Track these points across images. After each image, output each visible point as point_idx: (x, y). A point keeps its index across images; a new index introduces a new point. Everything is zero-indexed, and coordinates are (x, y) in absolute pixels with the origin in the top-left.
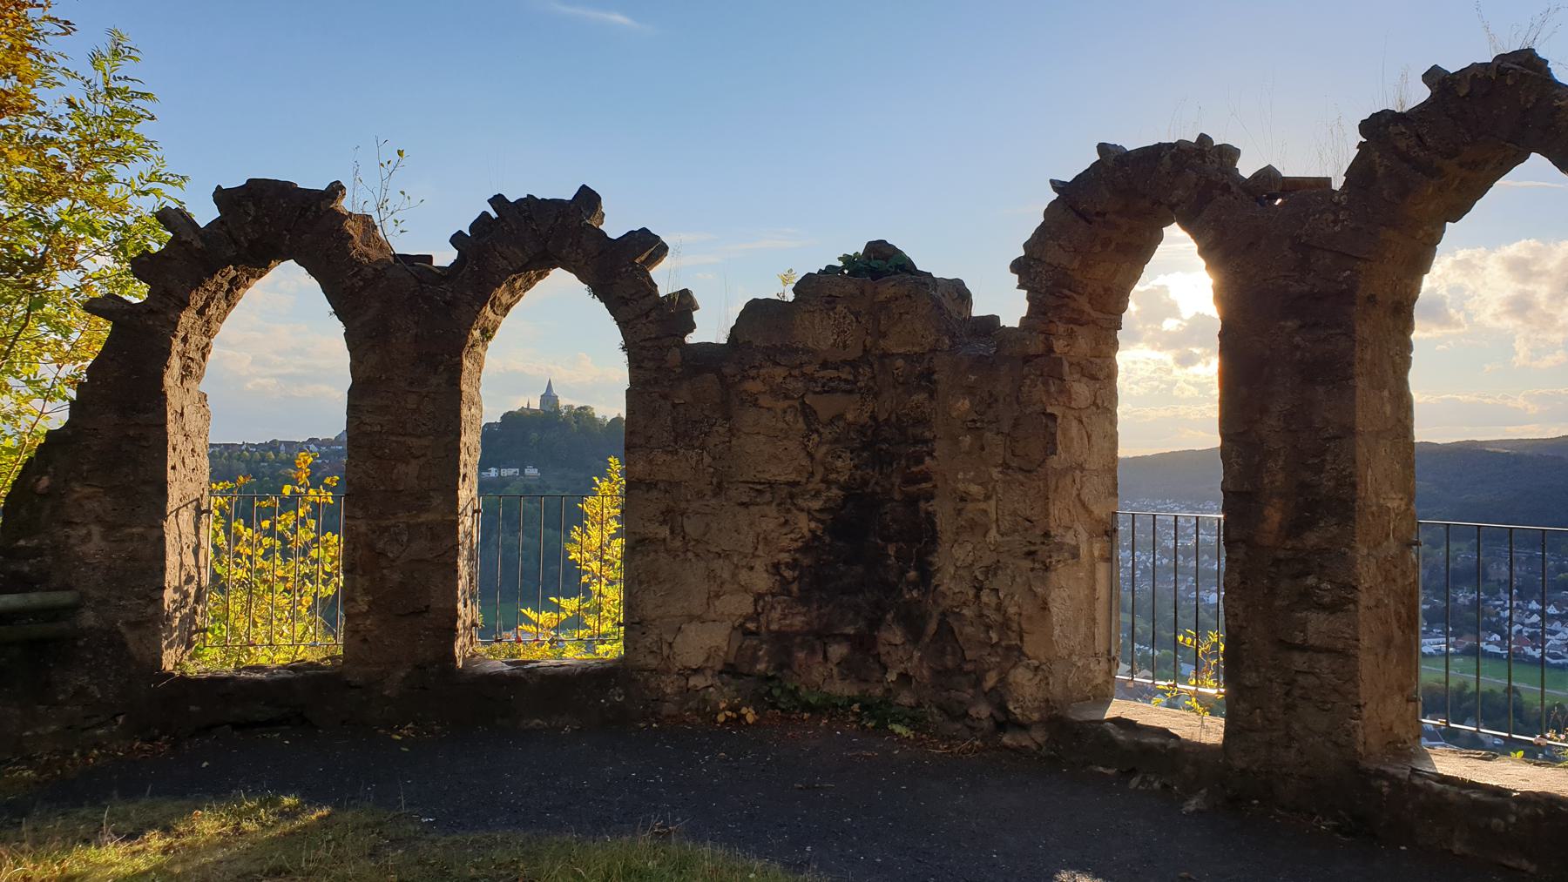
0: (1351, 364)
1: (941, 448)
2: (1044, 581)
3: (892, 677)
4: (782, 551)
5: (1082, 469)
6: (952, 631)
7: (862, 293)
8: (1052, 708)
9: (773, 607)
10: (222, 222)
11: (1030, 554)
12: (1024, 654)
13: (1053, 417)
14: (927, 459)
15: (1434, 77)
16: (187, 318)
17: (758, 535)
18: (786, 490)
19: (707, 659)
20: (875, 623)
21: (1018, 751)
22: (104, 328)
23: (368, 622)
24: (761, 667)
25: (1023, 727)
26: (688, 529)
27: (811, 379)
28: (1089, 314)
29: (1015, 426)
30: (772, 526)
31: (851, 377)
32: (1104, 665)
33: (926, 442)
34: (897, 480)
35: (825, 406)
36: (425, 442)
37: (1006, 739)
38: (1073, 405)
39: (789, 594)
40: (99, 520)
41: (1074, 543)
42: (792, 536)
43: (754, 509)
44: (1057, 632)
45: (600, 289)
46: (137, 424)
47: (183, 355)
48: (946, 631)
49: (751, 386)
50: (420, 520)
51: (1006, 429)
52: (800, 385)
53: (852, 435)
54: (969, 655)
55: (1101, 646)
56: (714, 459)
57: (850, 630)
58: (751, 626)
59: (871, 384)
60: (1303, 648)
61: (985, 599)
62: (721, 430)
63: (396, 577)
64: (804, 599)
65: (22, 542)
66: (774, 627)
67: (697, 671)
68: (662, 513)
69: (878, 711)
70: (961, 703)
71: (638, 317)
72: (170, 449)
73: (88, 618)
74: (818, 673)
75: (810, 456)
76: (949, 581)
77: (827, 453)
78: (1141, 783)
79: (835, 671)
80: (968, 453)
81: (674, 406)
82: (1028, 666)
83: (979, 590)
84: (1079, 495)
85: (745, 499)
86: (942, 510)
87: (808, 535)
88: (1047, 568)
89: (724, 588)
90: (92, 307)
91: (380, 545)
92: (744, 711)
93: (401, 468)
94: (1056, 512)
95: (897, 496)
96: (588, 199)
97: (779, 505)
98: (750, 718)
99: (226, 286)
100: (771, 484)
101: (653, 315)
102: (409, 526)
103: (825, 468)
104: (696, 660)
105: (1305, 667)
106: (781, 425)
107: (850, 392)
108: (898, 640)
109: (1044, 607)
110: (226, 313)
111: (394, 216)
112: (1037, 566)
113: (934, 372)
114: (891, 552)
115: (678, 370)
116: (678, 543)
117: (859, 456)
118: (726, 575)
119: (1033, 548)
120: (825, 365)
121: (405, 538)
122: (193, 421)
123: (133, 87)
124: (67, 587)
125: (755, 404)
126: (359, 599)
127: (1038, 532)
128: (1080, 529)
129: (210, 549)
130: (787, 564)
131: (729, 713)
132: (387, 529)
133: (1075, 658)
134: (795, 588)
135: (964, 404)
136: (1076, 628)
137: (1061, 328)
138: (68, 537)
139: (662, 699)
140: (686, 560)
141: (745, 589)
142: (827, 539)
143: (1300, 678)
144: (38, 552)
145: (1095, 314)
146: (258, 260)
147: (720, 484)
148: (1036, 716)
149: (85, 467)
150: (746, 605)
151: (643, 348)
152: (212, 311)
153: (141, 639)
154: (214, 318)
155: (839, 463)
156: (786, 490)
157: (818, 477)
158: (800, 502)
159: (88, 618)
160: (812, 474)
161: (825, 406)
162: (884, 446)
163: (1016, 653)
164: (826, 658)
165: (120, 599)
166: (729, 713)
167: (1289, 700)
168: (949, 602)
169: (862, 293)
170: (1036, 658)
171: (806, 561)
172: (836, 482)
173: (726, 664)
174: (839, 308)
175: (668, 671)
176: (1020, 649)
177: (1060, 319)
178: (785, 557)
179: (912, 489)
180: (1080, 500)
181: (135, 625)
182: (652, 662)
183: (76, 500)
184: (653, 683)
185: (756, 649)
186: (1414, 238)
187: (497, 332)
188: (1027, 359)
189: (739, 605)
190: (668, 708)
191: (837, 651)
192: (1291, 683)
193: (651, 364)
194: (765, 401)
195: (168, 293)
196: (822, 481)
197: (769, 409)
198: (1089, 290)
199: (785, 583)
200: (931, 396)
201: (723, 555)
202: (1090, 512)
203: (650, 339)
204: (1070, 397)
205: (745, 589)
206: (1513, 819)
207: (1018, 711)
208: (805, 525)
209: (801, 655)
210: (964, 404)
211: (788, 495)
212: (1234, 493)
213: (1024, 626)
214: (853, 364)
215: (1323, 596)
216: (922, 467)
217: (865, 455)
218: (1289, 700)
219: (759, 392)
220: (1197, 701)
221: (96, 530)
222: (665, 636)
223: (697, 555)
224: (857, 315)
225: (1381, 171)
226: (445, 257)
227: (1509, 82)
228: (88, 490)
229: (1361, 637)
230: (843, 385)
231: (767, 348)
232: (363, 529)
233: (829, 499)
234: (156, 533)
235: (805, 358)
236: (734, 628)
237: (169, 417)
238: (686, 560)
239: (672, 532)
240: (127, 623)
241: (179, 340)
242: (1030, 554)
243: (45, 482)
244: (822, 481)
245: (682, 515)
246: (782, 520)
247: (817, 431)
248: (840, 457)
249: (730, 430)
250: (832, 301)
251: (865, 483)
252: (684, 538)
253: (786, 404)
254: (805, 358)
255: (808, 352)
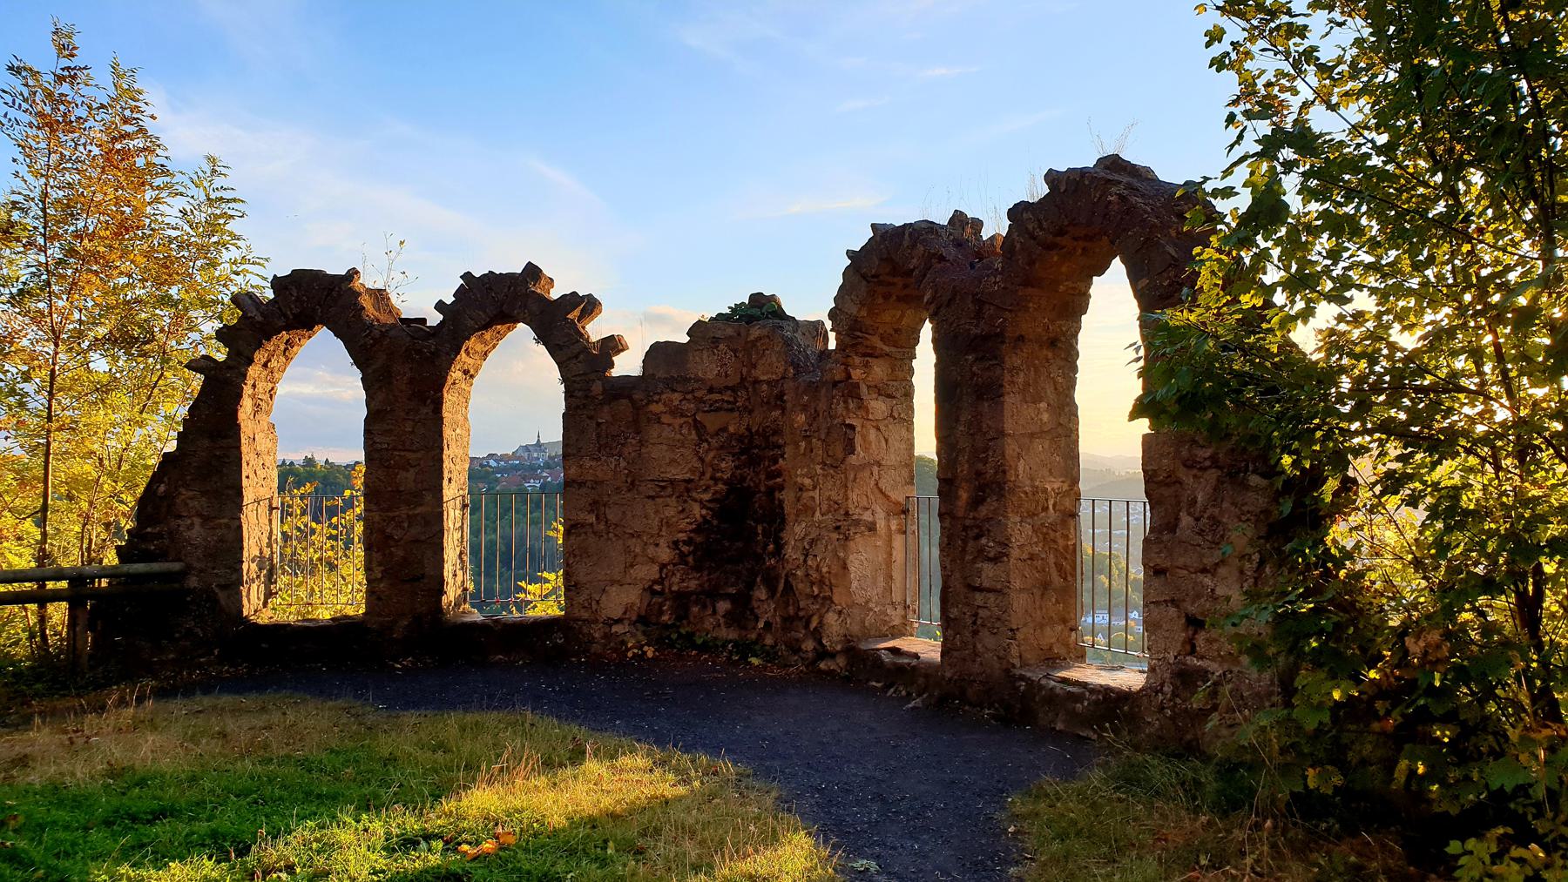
0: (1002, 386)
1: (789, 450)
2: (845, 548)
3: (761, 625)
4: (680, 532)
5: (879, 465)
6: (792, 586)
7: (739, 334)
8: (849, 641)
9: (673, 574)
10: (276, 302)
11: (838, 528)
12: (832, 602)
13: (852, 427)
14: (780, 460)
15: (1052, 177)
16: (254, 371)
17: (662, 519)
18: (683, 485)
19: (625, 613)
20: (751, 586)
21: (830, 673)
22: (197, 381)
23: (382, 585)
24: (665, 618)
25: (832, 655)
26: (610, 517)
27: (701, 400)
28: (882, 349)
29: (828, 434)
30: (672, 513)
31: (732, 399)
32: (900, 611)
33: (779, 447)
34: (763, 477)
35: (712, 422)
36: (419, 455)
37: (822, 666)
38: (870, 417)
39: (686, 563)
40: (199, 515)
41: (870, 519)
42: (688, 520)
43: (659, 500)
44: (855, 585)
45: (543, 337)
46: (221, 447)
47: (253, 397)
48: (789, 587)
49: (654, 408)
50: (416, 512)
51: (823, 437)
52: (692, 406)
53: (734, 443)
54: (802, 604)
55: (897, 597)
56: (628, 463)
57: (732, 590)
58: (657, 587)
59: (747, 404)
60: (980, 589)
61: (810, 563)
62: (634, 442)
63: (401, 553)
64: (697, 568)
65: (149, 530)
66: (675, 588)
67: (619, 621)
68: (590, 504)
69: (745, 649)
70: (797, 640)
71: (569, 359)
72: (244, 465)
73: (193, 582)
74: (709, 622)
75: (702, 460)
76: (792, 553)
77: (714, 457)
78: (895, 692)
79: (722, 621)
80: (804, 454)
81: (599, 424)
82: (834, 611)
83: (807, 556)
84: (877, 484)
85: (652, 493)
86: (787, 497)
87: (700, 520)
88: (847, 539)
89: (638, 559)
90: (193, 366)
91: (388, 530)
92: (646, 648)
93: (402, 474)
94: (855, 497)
95: (763, 489)
96: (532, 271)
97: (678, 497)
98: (650, 654)
99: (282, 347)
100: (672, 482)
101: (582, 356)
102: (408, 516)
103: (713, 469)
104: (617, 613)
105: (981, 604)
106: (678, 436)
107: (732, 410)
108: (763, 597)
109: (845, 567)
110: (286, 365)
111: (397, 291)
112: (841, 537)
113: (785, 394)
114: (760, 530)
115: (601, 398)
116: (602, 526)
117: (739, 459)
118: (638, 550)
119: (839, 524)
120: (711, 390)
121: (406, 525)
122: (263, 443)
123: (227, 195)
124: (179, 560)
125: (659, 421)
126: (375, 569)
127: (842, 512)
128: (879, 510)
129: (279, 534)
130: (684, 542)
131: (636, 651)
132: (393, 518)
133: (871, 605)
134: (690, 559)
135: (801, 418)
136: (875, 582)
137: (857, 360)
138: (179, 526)
139: (592, 640)
140: (609, 539)
141: (653, 560)
142: (715, 522)
143: (980, 611)
144: (160, 536)
145: (887, 349)
146: (306, 323)
147: (633, 483)
148: (839, 648)
149: (189, 478)
150: (653, 572)
151: (574, 382)
152: (273, 364)
153: (229, 598)
154: (276, 369)
155: (723, 465)
156: (683, 485)
157: (708, 475)
158: (694, 494)
159: (193, 582)
160: (703, 474)
161: (712, 422)
162: (756, 451)
163: (828, 602)
164: (714, 612)
165: (214, 569)
166: (636, 651)
167: (975, 627)
168: (790, 566)
169: (739, 334)
170: (840, 605)
171: (699, 539)
172: (721, 479)
173: (639, 616)
174: (721, 346)
175: (596, 621)
176: (830, 599)
177: (856, 354)
178: (682, 536)
179: (771, 483)
180: (878, 488)
181: (224, 587)
182: (585, 615)
183: (183, 500)
184: (585, 630)
185: (661, 605)
186: (1057, 291)
187: (480, 372)
188: (835, 384)
189: (647, 572)
190: (596, 648)
191: (723, 606)
192: (976, 615)
193: (581, 393)
194: (666, 419)
195: (239, 354)
196: (711, 478)
197: (669, 425)
198: (881, 331)
199: (682, 556)
200: (783, 413)
201: (636, 535)
202: (887, 497)
203: (580, 375)
204: (867, 412)
205: (653, 560)
206: (1086, 704)
207: (828, 644)
208: (697, 511)
209: (695, 609)
210: (801, 418)
211: (684, 489)
212: (944, 479)
213: (833, 581)
214: (733, 389)
215: (989, 552)
216: (777, 466)
217: (743, 458)
218: (975, 627)
219: (662, 412)
220: (187, 490)
221: (197, 521)
222: (594, 595)
223: (616, 535)
224: (735, 351)
225: (1018, 246)
226: (435, 318)
227: (1087, 183)
228: (191, 493)
229: (1012, 581)
230: (725, 406)
231: (666, 378)
232: (377, 518)
233: (716, 492)
234: (235, 524)
235: (696, 386)
236: (644, 590)
237: (243, 441)
238: (609, 539)
239: (597, 518)
240: (220, 586)
241: (249, 386)
242: (838, 528)
243: (162, 488)
244: (711, 478)
245: (605, 506)
246: (680, 508)
247: (707, 441)
248: (724, 460)
249: (640, 441)
250: (716, 341)
251: (743, 479)
252: (606, 522)
253: (682, 420)
254: (696, 386)
255: (698, 381)
